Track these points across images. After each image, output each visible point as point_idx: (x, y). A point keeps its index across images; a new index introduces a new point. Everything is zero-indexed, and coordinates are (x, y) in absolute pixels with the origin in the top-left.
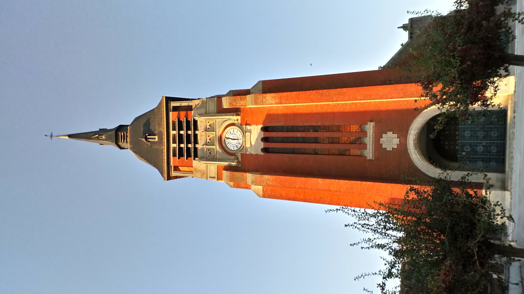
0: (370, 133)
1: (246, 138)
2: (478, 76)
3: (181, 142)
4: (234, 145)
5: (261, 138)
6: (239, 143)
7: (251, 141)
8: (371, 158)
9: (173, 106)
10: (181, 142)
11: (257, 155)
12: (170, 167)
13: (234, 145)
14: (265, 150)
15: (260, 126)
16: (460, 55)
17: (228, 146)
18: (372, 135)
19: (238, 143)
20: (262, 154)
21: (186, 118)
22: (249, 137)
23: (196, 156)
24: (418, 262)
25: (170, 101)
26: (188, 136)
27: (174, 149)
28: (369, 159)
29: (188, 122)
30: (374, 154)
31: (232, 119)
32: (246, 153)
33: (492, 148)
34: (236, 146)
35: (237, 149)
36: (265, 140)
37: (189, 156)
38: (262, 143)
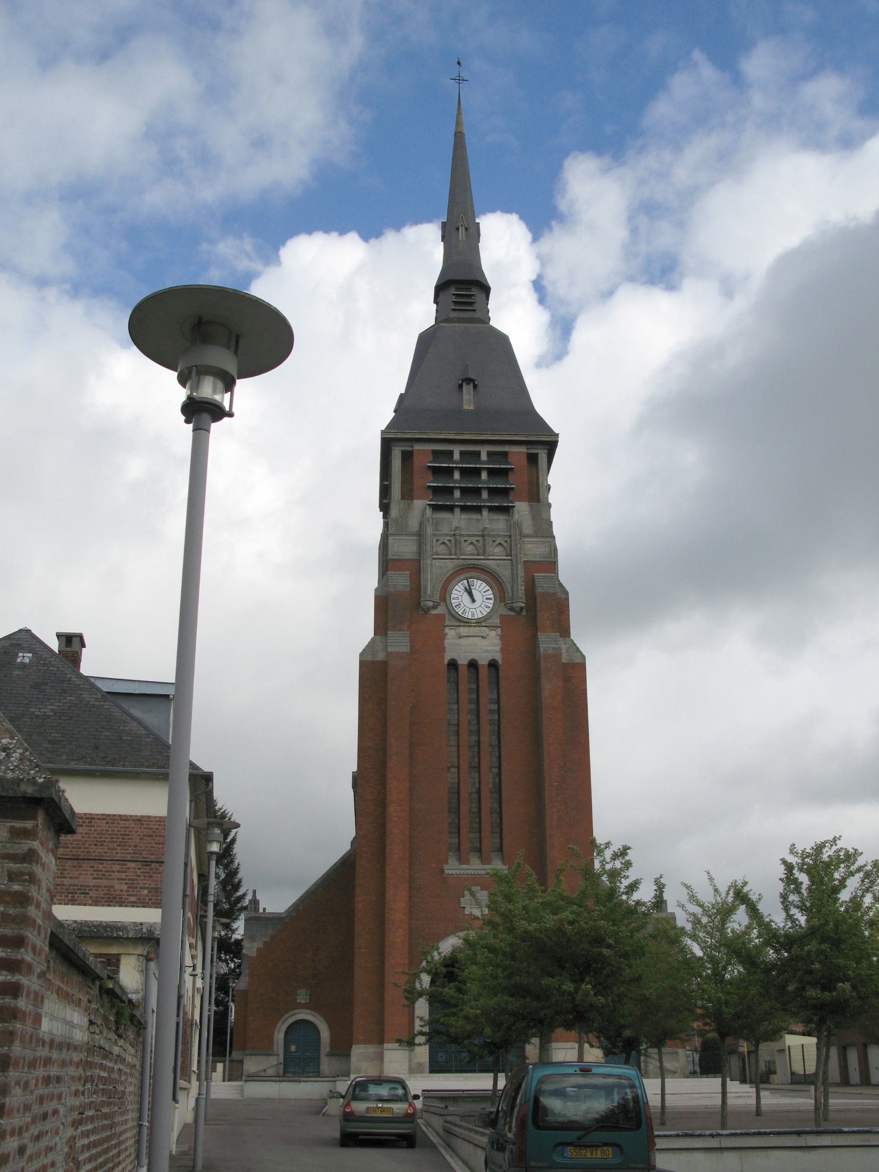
0: (468, 869)
1: (477, 628)
2: (847, 986)
3: (466, 472)
4: (460, 600)
5: (476, 658)
6: (465, 609)
7: (471, 638)
8: (446, 872)
9: (537, 454)
10: (466, 472)
11: (444, 650)
12: (409, 444)
13: (460, 600)
14: (453, 665)
15: (498, 657)
16: (590, 981)
17: (459, 584)
18: (469, 873)
19: (465, 608)
20: (446, 662)
21: (514, 488)
22: (479, 634)
23: (436, 508)
24: (843, 851)
25: (548, 448)
26: (477, 491)
27: (91, 830)
28: (445, 868)
29: (505, 492)
30: (454, 877)
31: (118, 881)
32: (445, 626)
33: (444, 1056)
34: (460, 604)
35: (454, 605)
36: (473, 665)
37: (436, 491)
38: (486, 663)
